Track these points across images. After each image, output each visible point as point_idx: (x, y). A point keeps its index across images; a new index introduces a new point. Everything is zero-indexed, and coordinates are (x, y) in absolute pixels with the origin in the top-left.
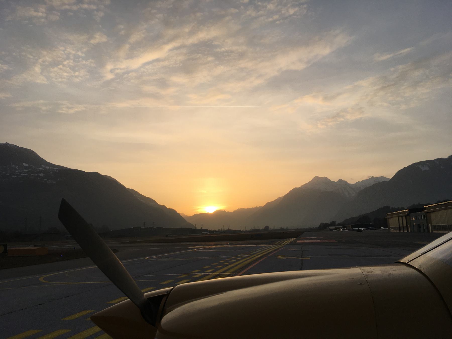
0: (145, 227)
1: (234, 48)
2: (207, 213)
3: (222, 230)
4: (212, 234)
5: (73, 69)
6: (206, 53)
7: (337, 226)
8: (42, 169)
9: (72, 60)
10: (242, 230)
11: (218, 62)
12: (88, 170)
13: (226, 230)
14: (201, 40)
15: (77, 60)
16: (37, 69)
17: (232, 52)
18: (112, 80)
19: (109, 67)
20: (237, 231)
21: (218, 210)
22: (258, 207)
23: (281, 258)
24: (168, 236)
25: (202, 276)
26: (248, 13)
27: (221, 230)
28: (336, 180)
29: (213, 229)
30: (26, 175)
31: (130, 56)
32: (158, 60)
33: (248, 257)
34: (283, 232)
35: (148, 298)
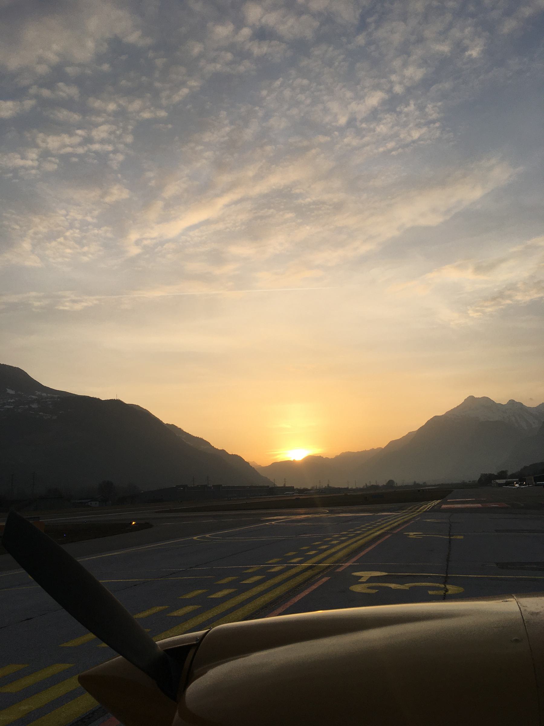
0: (195, 486)
1: (326, 197)
2: (292, 460)
3: (318, 488)
4: (300, 494)
5: (80, 242)
6: (282, 207)
7: (509, 479)
8: (36, 397)
9: (76, 228)
10: (349, 488)
11: (301, 220)
12: (104, 397)
13: (324, 487)
14: (274, 187)
15: (85, 228)
16: (26, 245)
17: (323, 203)
18: (138, 256)
19: (134, 236)
20: (342, 489)
21: (310, 455)
22: (375, 448)
23: (414, 537)
24: (231, 498)
25: (283, 569)
26: (346, 140)
27: (315, 488)
28: (504, 402)
29: (302, 487)
30: (12, 407)
31: (164, 219)
32: (207, 222)
33: (360, 534)
34: (419, 491)
35: (167, 651)
